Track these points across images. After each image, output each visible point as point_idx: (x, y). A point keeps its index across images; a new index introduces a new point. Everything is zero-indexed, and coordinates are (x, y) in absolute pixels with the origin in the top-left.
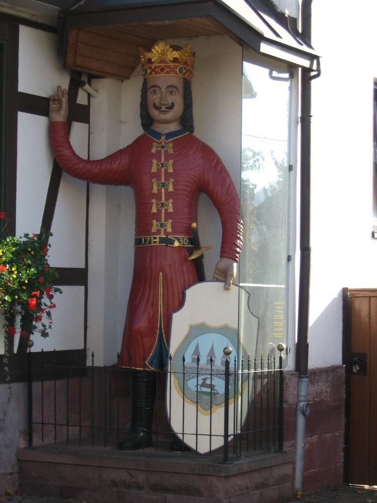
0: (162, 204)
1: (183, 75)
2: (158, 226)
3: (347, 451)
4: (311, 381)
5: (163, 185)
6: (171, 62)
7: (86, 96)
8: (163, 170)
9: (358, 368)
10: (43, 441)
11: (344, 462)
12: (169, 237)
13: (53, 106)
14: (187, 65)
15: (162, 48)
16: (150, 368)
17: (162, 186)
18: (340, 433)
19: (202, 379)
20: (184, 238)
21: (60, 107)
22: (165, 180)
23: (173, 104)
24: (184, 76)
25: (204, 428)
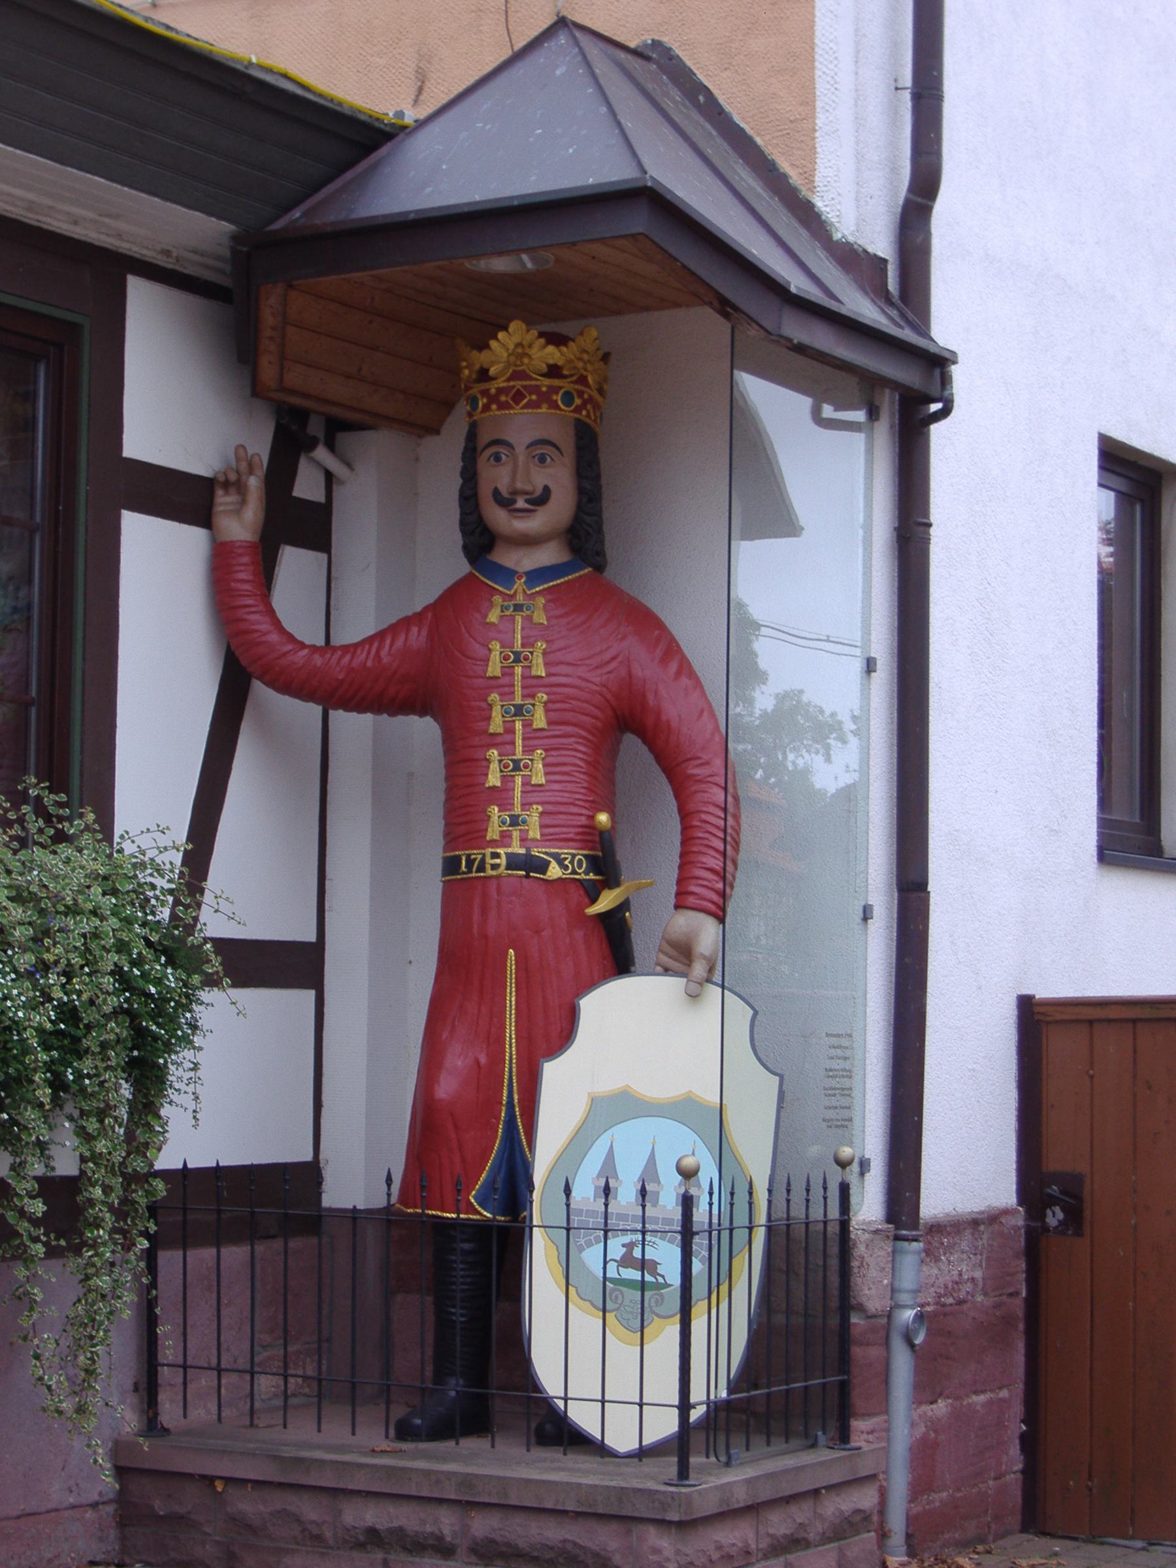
0: (516, 763)
1: (574, 411)
2: (504, 823)
3: (1029, 1443)
4: (927, 1252)
5: (519, 711)
6: (543, 375)
7: (321, 479)
8: (518, 670)
9: (1060, 1215)
10: (185, 1416)
11: (1023, 1472)
12: (535, 852)
13: (224, 501)
14: (587, 385)
15: (516, 339)
16: (479, 1213)
17: (515, 715)
18: (1012, 1394)
19: (623, 1246)
20: (574, 856)
21: (243, 502)
22: (524, 696)
23: (547, 490)
24: (577, 416)
25: (623, 1386)
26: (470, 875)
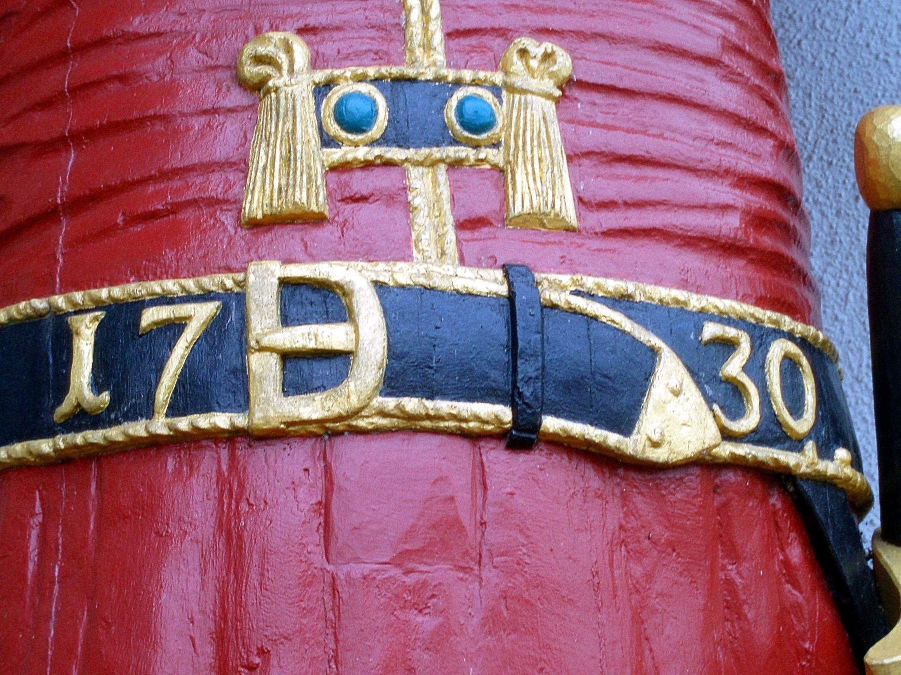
26: (138, 429)
